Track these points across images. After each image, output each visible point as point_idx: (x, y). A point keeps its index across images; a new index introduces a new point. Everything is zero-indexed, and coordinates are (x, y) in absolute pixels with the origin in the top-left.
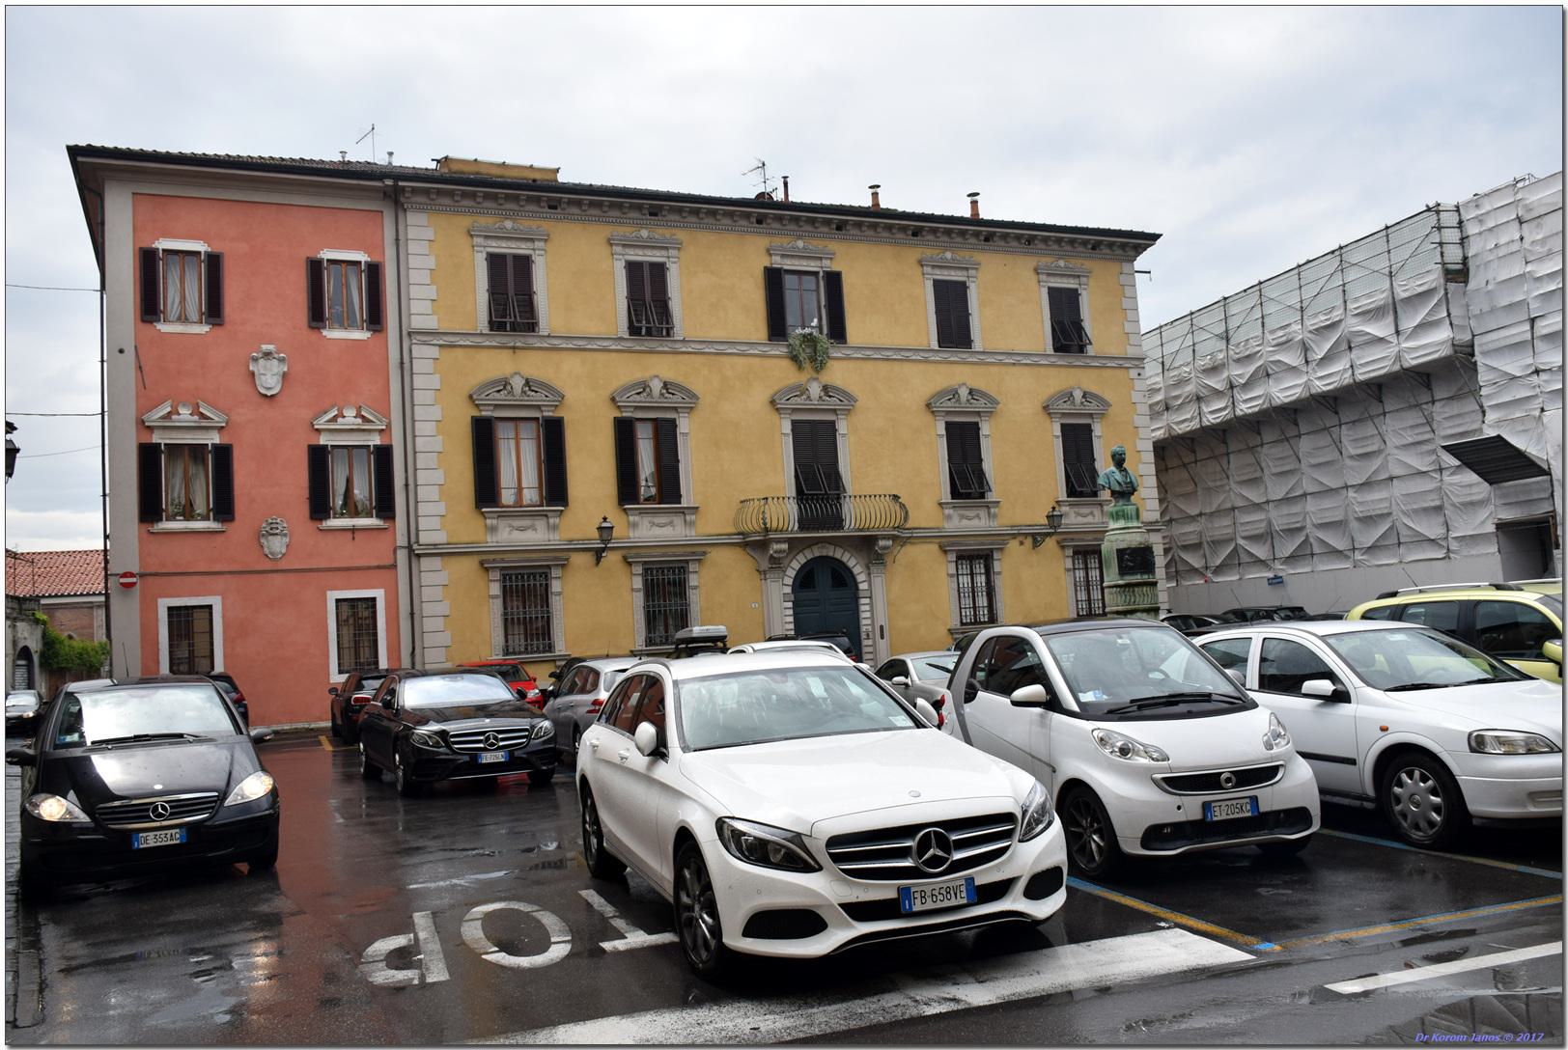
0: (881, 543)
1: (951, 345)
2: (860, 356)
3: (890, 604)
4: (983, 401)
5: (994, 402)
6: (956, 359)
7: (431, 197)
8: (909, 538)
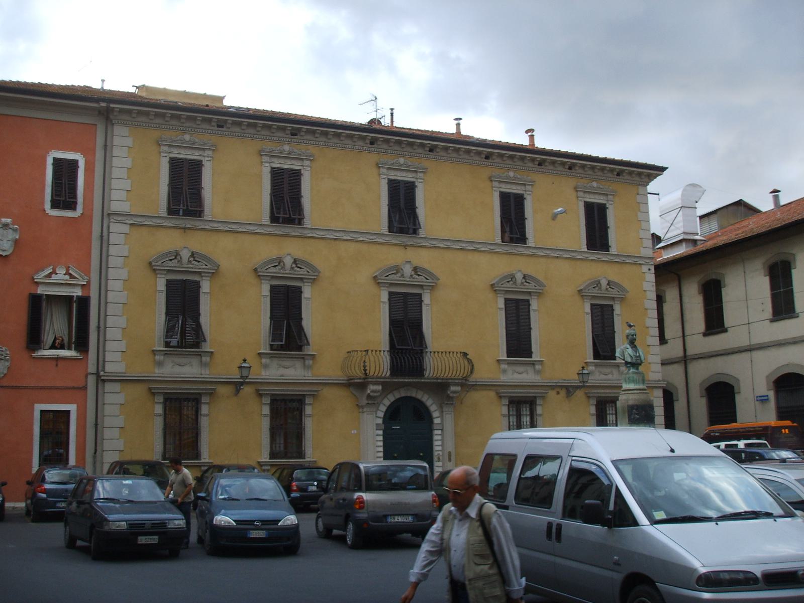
0: (453, 388)
5: (623, 289)
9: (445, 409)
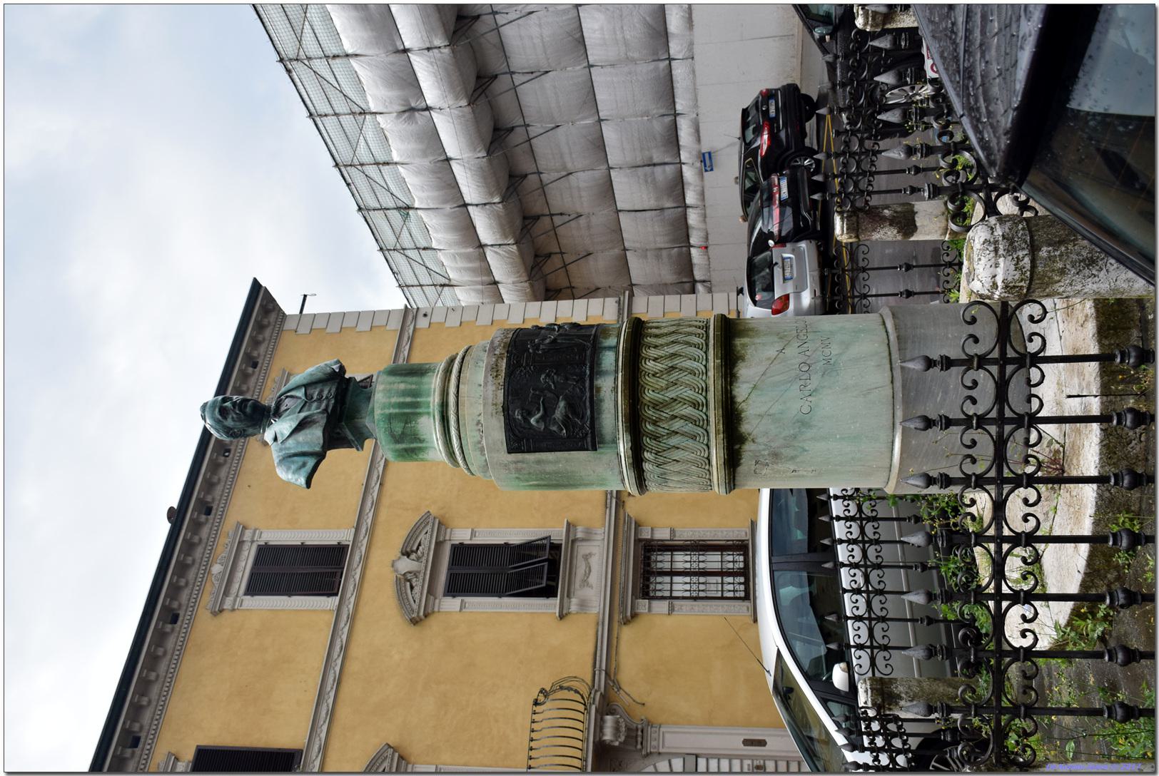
0: (608, 736)
1: (339, 574)
2: (325, 728)
3: (709, 721)
4: (422, 536)
5: (425, 519)
6: (358, 571)
7: (145, 703)
8: (607, 674)
9: (651, 745)
